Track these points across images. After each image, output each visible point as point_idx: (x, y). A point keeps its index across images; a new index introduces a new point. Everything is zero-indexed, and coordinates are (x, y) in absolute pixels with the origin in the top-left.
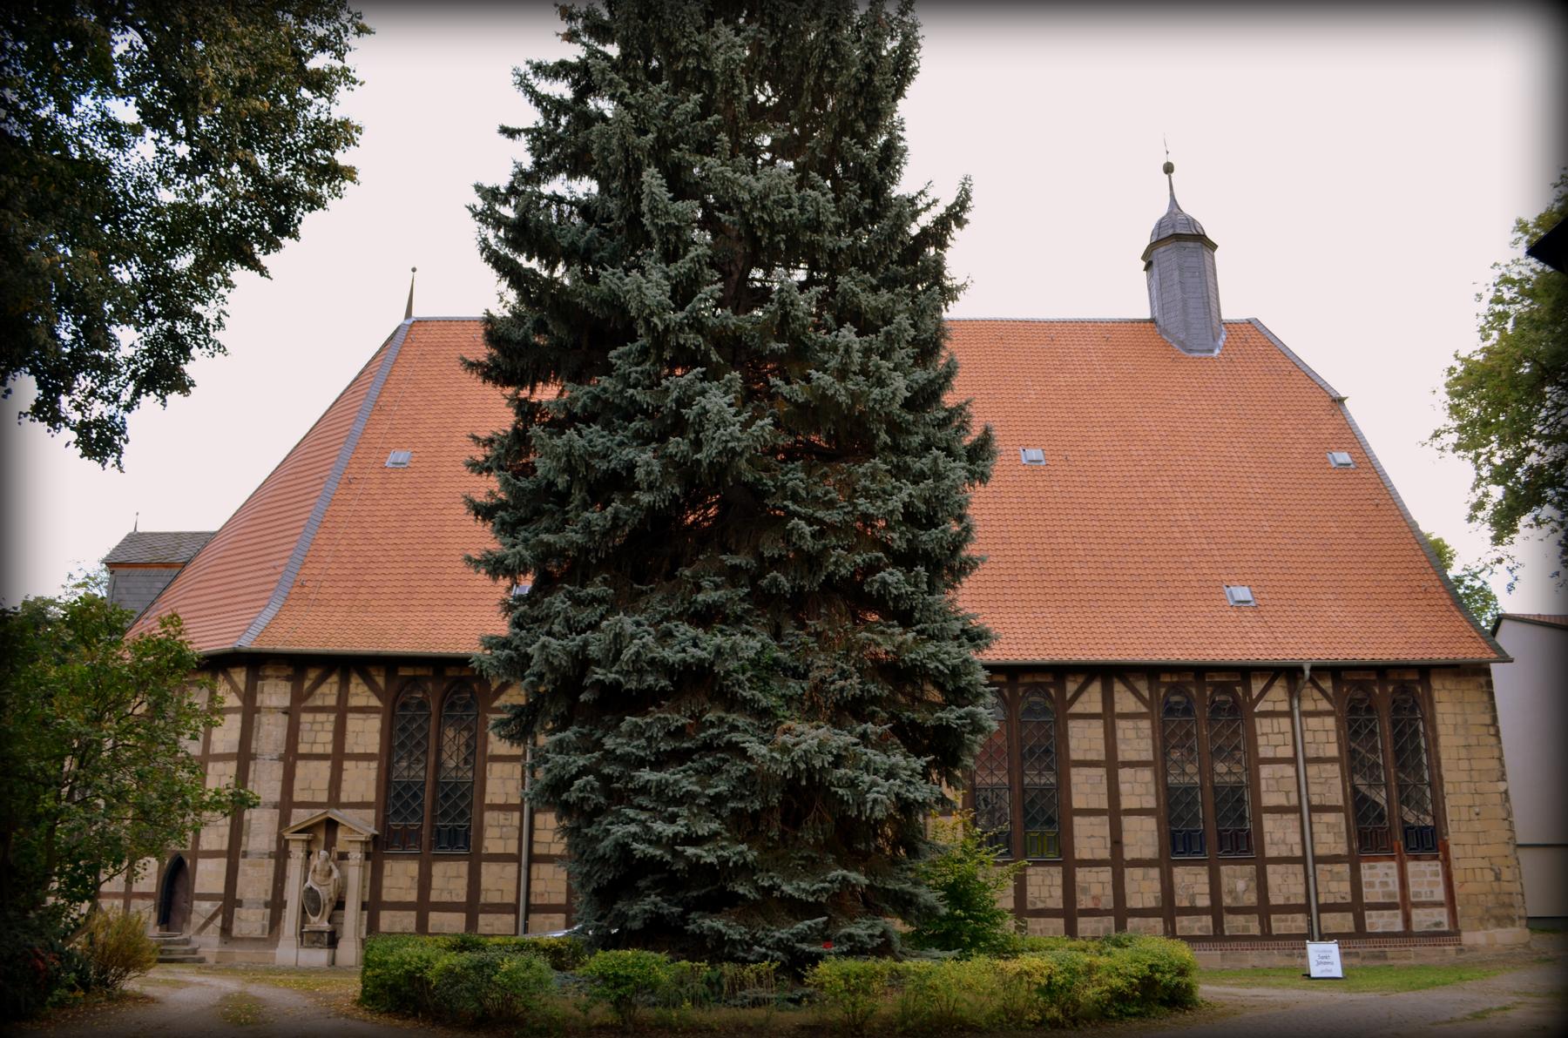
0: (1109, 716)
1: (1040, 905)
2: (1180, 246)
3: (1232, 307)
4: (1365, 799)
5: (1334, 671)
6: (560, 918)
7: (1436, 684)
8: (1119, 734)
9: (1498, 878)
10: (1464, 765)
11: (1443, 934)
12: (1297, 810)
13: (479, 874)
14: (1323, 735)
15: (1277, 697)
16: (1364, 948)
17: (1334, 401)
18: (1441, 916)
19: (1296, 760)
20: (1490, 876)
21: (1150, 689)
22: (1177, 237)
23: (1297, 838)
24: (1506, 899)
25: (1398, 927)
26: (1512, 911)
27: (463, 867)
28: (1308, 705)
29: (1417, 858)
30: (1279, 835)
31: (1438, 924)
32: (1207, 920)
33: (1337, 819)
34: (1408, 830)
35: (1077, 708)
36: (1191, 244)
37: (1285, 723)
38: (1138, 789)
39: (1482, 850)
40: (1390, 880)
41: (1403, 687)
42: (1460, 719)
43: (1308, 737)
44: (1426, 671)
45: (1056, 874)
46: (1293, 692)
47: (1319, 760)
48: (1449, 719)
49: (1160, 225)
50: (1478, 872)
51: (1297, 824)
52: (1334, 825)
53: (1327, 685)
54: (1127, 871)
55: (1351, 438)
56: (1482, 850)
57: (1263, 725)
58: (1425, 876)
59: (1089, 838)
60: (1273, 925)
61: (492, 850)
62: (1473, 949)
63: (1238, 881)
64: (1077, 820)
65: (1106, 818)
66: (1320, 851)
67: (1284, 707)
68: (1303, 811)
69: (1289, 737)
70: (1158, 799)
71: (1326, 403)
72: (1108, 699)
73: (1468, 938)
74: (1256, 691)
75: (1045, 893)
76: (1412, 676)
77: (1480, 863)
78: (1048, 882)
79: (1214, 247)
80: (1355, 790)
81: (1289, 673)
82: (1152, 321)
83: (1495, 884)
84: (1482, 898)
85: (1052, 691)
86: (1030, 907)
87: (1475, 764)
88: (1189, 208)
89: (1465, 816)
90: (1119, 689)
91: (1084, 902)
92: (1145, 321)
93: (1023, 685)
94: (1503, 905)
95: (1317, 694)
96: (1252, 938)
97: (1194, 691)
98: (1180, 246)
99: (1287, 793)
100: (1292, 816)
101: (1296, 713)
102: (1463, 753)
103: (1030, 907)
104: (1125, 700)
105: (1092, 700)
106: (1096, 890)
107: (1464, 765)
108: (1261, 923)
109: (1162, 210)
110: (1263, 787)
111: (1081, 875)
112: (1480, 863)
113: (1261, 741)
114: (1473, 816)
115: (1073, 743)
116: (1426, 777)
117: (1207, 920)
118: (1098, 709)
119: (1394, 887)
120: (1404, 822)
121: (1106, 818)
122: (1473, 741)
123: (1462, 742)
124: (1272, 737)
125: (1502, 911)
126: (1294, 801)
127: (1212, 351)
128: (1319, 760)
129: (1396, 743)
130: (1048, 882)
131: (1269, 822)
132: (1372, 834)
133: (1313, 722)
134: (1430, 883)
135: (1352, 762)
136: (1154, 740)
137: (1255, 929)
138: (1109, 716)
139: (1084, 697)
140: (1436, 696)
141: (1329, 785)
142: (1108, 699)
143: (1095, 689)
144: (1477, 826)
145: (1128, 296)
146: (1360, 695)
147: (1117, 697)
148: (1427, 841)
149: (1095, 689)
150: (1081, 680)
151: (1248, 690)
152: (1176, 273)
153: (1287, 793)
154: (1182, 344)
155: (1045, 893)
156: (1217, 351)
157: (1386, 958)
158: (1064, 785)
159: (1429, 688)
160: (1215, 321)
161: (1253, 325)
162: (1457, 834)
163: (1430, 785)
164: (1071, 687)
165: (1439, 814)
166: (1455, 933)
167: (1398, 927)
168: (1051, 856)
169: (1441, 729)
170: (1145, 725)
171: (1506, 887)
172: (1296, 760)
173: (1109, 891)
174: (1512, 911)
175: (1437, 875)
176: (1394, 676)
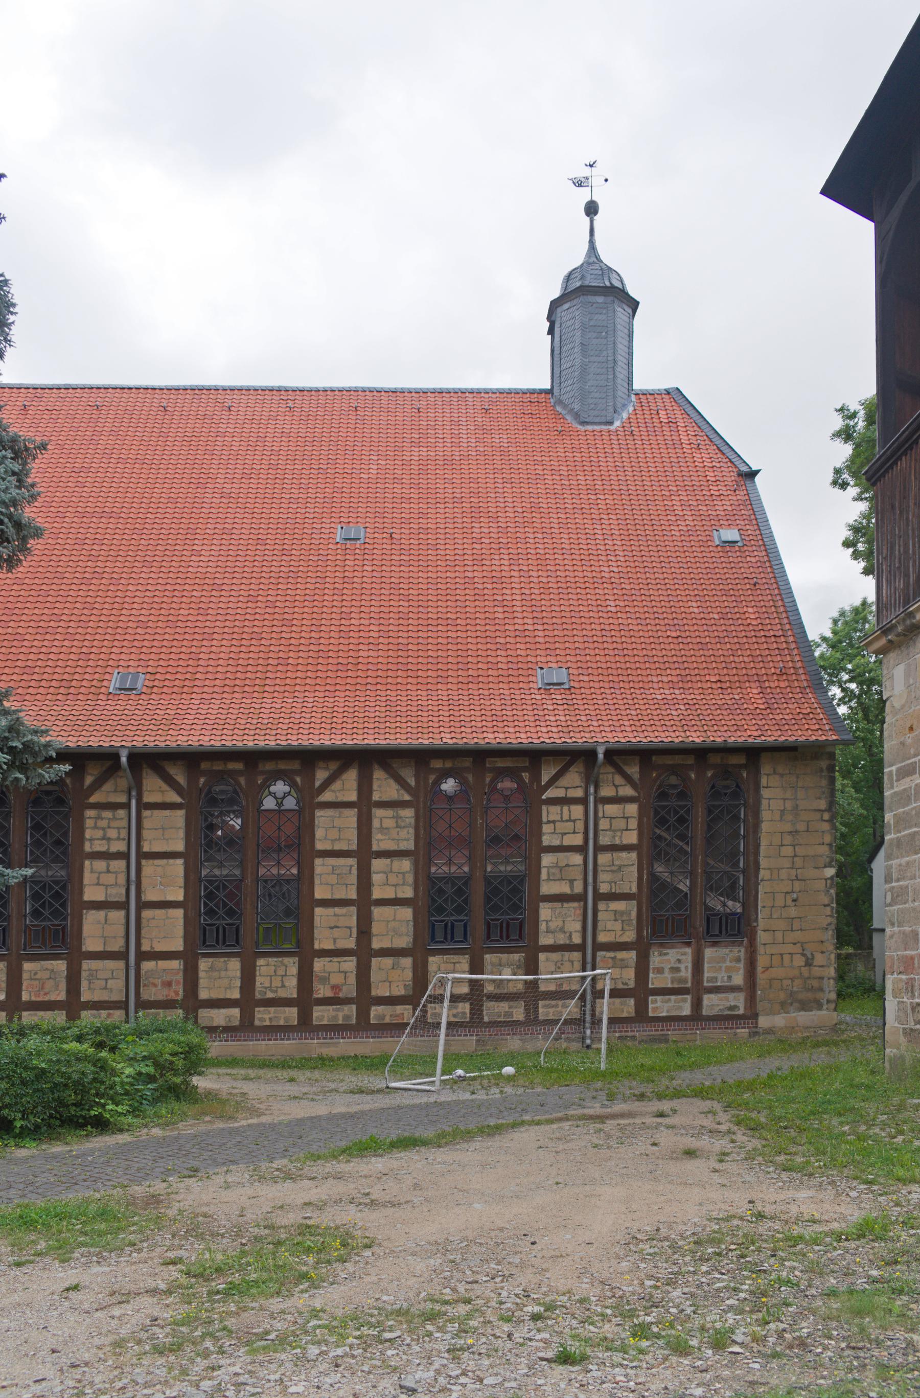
0: (364, 806)
1: (270, 995)
2: (593, 303)
3: (648, 374)
4: (664, 885)
5: (645, 755)
6: (542, 988)
7: (766, 769)
8: (376, 823)
9: (809, 963)
10: (787, 851)
11: (738, 1017)
12: (581, 898)
13: (368, 967)
14: (623, 822)
15: (572, 783)
16: (639, 1031)
17: (740, 474)
18: (738, 1001)
19: (587, 851)
20: (799, 961)
21: (417, 777)
22: (584, 290)
23: (578, 926)
24: (815, 983)
25: (686, 1011)
26: (819, 995)
27: (61, 966)
28: (607, 791)
29: (715, 944)
30: (556, 923)
31: (732, 1008)
32: (351, 1010)
33: (629, 908)
34: (710, 916)
35: (327, 796)
36: (600, 299)
37: (577, 811)
38: (394, 879)
39: (797, 936)
40: (682, 967)
41: (726, 772)
42: (789, 805)
43: (603, 824)
44: (754, 754)
45: (292, 966)
46: (591, 779)
47: (614, 848)
48: (776, 805)
49: (568, 278)
50: (786, 958)
51: (580, 912)
52: (622, 913)
53: (634, 770)
54: (375, 961)
55: (753, 517)
56: (797, 936)
57: (549, 813)
58: (723, 963)
59: (331, 928)
60: (541, 1010)
61: (91, 949)
62: (770, 1031)
63: (504, 972)
64: (318, 911)
65: (354, 909)
66: (602, 938)
67: (579, 793)
68: (589, 899)
69: (580, 826)
70: (416, 890)
71: (730, 477)
72: (365, 787)
73: (764, 1021)
74: (545, 778)
75: (277, 983)
76: (741, 760)
77: (790, 948)
78: (281, 972)
79: (634, 305)
80: (653, 877)
81: (583, 757)
82: (550, 392)
83: (805, 971)
84: (787, 982)
85: (298, 779)
86: (258, 996)
87: (800, 851)
88: (607, 257)
89: (780, 901)
90: (379, 775)
91: (322, 991)
92: (541, 391)
93: (262, 773)
94: (812, 989)
95: (619, 780)
96: (517, 1023)
97: (470, 778)
98: (593, 303)
99: (571, 882)
100: (576, 904)
101: (592, 799)
102: (788, 839)
103: (258, 996)
104: (385, 787)
105: (347, 787)
106: (336, 979)
107: (787, 851)
108: (527, 1010)
109: (578, 258)
110: (544, 874)
111: (319, 965)
112: (790, 948)
113: (546, 828)
114: (789, 902)
115: (319, 833)
116: (741, 865)
117: (351, 1010)
118: (353, 797)
119: (686, 972)
120: (707, 908)
121: (354, 909)
122: (801, 827)
123: (788, 827)
124: (559, 825)
125: (810, 995)
126: (578, 888)
127: (611, 423)
128: (614, 848)
129: (710, 828)
130: (281, 972)
131: (545, 911)
132: (666, 917)
133: (611, 809)
134: (728, 969)
135: (652, 849)
136: (417, 828)
137: (519, 1014)
138: (364, 806)
139: (337, 785)
140: (764, 781)
141: (623, 872)
142: (365, 787)
143: (351, 777)
144: (793, 912)
145: (528, 366)
146: (673, 780)
147: (375, 785)
148: (736, 928)
149: (351, 777)
150: (334, 766)
151: (537, 777)
152: (579, 334)
153: (571, 882)
154: (577, 416)
155: (277, 983)
156: (617, 424)
157: (667, 1041)
158: (306, 876)
159: (758, 773)
160: (621, 391)
161: (675, 395)
162: (764, 919)
163: (744, 872)
164: (321, 775)
165: (750, 903)
166: (752, 1016)
167: (686, 1011)
168: (287, 947)
169: (765, 815)
170: (408, 814)
171: (816, 971)
172: (587, 851)
173: (352, 979)
174: (819, 995)
175: (738, 960)
176: (715, 759)
